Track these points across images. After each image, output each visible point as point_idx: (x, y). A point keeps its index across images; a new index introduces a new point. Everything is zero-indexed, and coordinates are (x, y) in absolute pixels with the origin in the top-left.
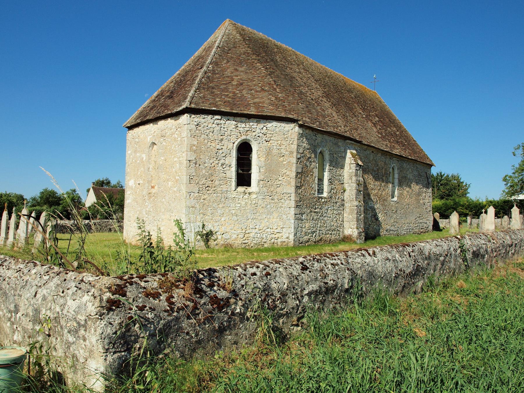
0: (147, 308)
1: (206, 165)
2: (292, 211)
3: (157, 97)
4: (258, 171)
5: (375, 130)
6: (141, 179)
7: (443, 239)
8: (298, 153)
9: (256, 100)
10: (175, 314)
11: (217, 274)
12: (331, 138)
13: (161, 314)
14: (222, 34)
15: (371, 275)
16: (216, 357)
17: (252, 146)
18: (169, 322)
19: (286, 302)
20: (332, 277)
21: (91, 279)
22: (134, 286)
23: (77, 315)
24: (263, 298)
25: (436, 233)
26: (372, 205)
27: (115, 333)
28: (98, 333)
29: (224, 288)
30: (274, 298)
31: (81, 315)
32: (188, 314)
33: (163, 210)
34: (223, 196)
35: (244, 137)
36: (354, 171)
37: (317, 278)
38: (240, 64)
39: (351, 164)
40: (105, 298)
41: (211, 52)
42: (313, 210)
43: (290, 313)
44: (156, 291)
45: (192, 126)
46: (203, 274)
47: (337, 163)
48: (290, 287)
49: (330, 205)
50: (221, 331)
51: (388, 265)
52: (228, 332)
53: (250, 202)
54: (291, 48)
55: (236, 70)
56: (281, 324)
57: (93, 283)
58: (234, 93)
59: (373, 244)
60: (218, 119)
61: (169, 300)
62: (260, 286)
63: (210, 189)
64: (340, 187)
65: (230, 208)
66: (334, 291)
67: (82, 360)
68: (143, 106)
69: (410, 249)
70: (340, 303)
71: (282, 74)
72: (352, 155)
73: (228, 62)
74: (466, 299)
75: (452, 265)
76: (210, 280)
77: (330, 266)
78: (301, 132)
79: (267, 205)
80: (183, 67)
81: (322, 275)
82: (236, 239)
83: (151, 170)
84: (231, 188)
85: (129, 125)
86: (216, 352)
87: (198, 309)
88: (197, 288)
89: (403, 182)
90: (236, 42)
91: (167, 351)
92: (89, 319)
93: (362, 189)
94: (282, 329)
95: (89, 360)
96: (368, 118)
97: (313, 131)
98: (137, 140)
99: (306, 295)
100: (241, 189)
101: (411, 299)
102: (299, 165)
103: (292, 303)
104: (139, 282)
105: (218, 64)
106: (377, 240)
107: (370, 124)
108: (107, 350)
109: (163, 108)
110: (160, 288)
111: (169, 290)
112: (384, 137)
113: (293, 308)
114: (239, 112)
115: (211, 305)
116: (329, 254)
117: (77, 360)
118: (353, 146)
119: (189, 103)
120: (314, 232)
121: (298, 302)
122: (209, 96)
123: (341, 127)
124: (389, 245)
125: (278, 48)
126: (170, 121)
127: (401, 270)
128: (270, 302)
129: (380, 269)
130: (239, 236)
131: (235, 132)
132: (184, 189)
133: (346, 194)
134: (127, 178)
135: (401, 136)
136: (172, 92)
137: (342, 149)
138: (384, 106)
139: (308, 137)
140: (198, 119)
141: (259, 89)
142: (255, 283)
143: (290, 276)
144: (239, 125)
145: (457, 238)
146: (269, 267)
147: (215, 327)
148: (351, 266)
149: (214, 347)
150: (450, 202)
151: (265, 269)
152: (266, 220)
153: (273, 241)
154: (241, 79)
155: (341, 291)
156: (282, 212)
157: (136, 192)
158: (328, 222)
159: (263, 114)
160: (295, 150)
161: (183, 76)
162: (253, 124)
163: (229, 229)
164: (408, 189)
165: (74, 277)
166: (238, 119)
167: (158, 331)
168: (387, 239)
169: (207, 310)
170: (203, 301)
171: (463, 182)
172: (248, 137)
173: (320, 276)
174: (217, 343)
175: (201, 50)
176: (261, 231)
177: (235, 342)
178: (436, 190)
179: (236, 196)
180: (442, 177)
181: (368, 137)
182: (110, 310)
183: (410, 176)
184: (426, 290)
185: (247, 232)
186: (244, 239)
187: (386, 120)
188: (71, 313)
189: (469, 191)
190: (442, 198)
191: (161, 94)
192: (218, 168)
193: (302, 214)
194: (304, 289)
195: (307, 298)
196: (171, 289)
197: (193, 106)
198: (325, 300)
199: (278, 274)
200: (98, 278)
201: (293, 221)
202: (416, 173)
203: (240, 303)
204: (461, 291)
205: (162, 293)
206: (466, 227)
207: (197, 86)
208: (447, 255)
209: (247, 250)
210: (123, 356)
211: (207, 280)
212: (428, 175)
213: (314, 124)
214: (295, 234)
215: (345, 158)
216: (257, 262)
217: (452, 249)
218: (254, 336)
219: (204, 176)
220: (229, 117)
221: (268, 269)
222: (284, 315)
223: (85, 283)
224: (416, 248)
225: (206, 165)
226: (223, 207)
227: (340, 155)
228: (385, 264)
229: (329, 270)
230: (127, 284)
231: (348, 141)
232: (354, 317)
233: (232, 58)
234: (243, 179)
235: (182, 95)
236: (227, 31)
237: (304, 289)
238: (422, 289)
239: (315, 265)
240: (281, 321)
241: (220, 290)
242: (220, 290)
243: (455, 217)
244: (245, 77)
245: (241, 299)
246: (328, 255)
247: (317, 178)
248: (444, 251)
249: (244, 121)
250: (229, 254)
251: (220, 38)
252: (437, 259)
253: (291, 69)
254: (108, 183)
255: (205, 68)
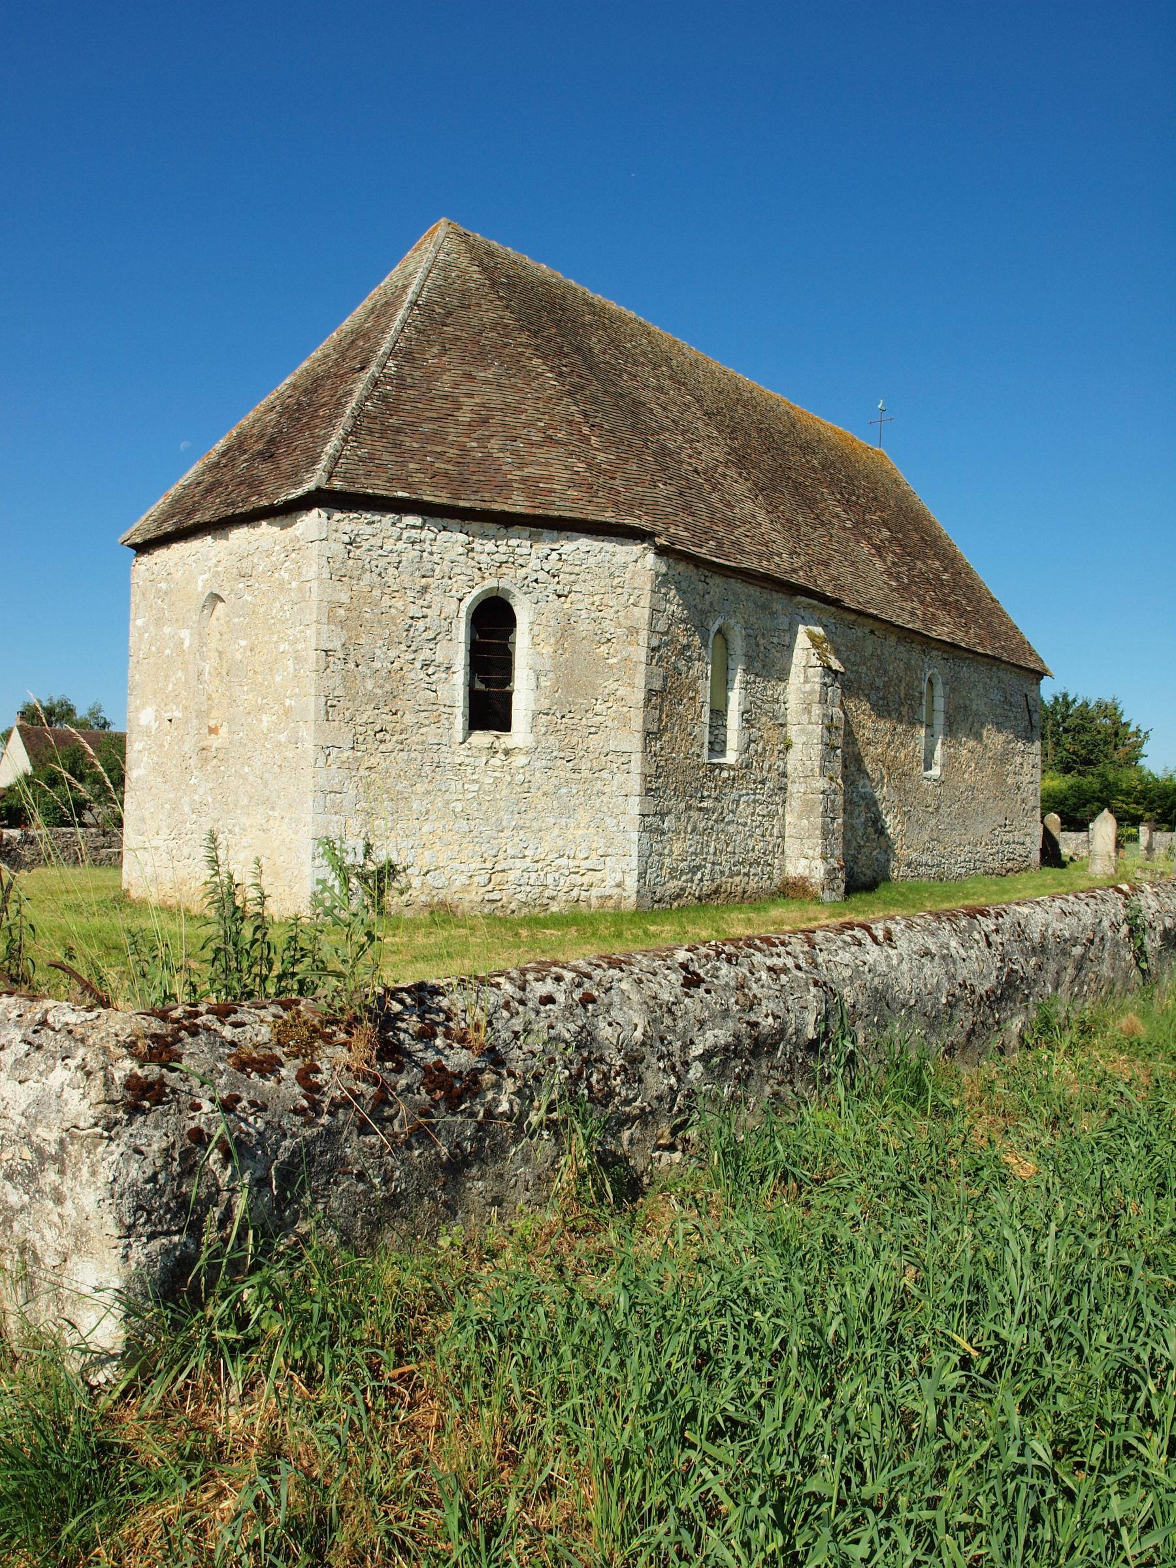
0: (244, 1103)
1: (377, 665)
2: (634, 806)
3: (224, 454)
4: (533, 686)
5: (879, 565)
6: (177, 705)
7: (1082, 895)
8: (652, 631)
9: (529, 471)
10: (325, 1119)
11: (445, 1003)
12: (752, 590)
13: (285, 1121)
14: (425, 265)
15: (881, 1000)
16: (444, 1242)
17: (516, 609)
18: (309, 1143)
19: (640, 1081)
20: (771, 1005)
21: (72, 1018)
22: (203, 1037)
23: (35, 1127)
24: (574, 1068)
25: (1051, 873)
26: (868, 789)
27: (153, 1179)
28: (101, 1180)
29: (463, 1041)
30: (605, 1068)
31: (48, 1126)
32: (363, 1120)
33: (246, 801)
34: (427, 760)
35: (491, 583)
36: (817, 687)
37: (727, 1010)
38: (482, 358)
39: (807, 666)
40: (119, 1075)
41: (391, 318)
42: (695, 803)
43: (651, 1113)
44: (268, 1052)
45: (333, 545)
46: (401, 1002)
47: (769, 664)
48: (651, 1038)
49: (744, 788)
50: (456, 1168)
51: (927, 971)
52: (474, 1170)
53: (508, 778)
54: (632, 314)
55: (469, 377)
56: (625, 1143)
57: (80, 1030)
58: (462, 448)
59: (871, 904)
60: (414, 527)
61: (304, 1077)
62: (567, 1036)
63: (388, 737)
64: (775, 734)
65: (447, 796)
66: (775, 1047)
67: (50, 1260)
68: (181, 482)
69: (989, 924)
70: (791, 1082)
71: (606, 392)
72: (812, 640)
73: (444, 351)
74: (1146, 1067)
75: (1105, 970)
76: (422, 1017)
77: (764, 975)
78: (664, 570)
79: (557, 788)
80: (305, 364)
81: (742, 1000)
82: (465, 888)
83: (207, 676)
84: (451, 736)
85: (139, 540)
86: (443, 1229)
87: (390, 1105)
88: (385, 1042)
89: (960, 722)
90: (469, 290)
91: (303, 1227)
92: (73, 1137)
93: (839, 742)
94: (627, 1159)
95: (75, 1258)
96: (860, 530)
97: (697, 566)
98: (163, 585)
99: (695, 1058)
100: (481, 738)
101: (990, 1068)
102: (656, 670)
103: (657, 1082)
104: (216, 1025)
105: (414, 359)
106: (882, 892)
107: (865, 549)
108: (130, 1228)
109: (245, 491)
110: (280, 1043)
111: (304, 1049)
112: (906, 588)
113: (660, 1099)
114: (479, 505)
115: (428, 1093)
116: (762, 940)
117: (37, 1259)
118: (816, 615)
119: (325, 476)
120: (699, 868)
121: (673, 1080)
122: (386, 456)
123: (780, 555)
124: (930, 913)
125: (594, 314)
126: (266, 531)
127: (963, 986)
128: (594, 1079)
129: (906, 983)
130: (475, 879)
131: (465, 567)
132: (308, 738)
133: (793, 757)
134: (134, 701)
135: (955, 586)
136: (272, 441)
137: (783, 622)
138: (906, 495)
139: (684, 585)
140: (353, 526)
141: (538, 437)
142: (551, 1027)
143: (652, 1003)
144: (477, 544)
145: (1120, 891)
146: (589, 977)
147: (438, 1154)
148: (824, 976)
149: (436, 1213)
150: (1090, 782)
151: (579, 985)
152: (556, 831)
153: (575, 893)
154: (483, 405)
155: (796, 1046)
156: (605, 809)
157: (162, 746)
158: (739, 838)
159: (550, 513)
160: (643, 625)
161: (306, 392)
162: (519, 544)
163: (441, 858)
164: (971, 743)
165: (16, 1012)
166: (475, 526)
167: (277, 1170)
168: (910, 889)
169: (417, 1105)
170: (403, 1082)
171: (1127, 725)
172: (504, 583)
173: (737, 1002)
174: (445, 1203)
175: (360, 311)
176: (539, 865)
177: (494, 1198)
178: (1050, 745)
179: (467, 761)
180: (1067, 708)
181: (860, 586)
182: (134, 1110)
183: (979, 705)
184: (1031, 1042)
185: (498, 867)
186: (489, 888)
187: (912, 538)
188: (13, 1122)
189: (1144, 751)
190: (1067, 769)
191: (239, 446)
192: (412, 675)
193: (662, 815)
194: (692, 1043)
195: (701, 1068)
196: (310, 1045)
197: (337, 484)
198: (749, 1074)
199: (616, 999)
200: (94, 1014)
201: (635, 836)
202: (997, 697)
203: (509, 1085)
204: (1131, 1044)
205: (283, 1058)
206: (1135, 854)
207: (351, 422)
208: (1091, 942)
209: (503, 922)
210: (175, 1246)
211: (415, 1018)
212: (1031, 703)
213: (701, 547)
214: (642, 876)
215: (790, 648)
216: (555, 963)
217: (1106, 923)
218: (550, 1181)
219: (370, 697)
220: (446, 522)
221: (587, 984)
222: (635, 1118)
223: (53, 1029)
224: (1006, 921)
225: (377, 665)
226: (428, 792)
227: (775, 640)
228: (921, 969)
229: (762, 986)
230: (183, 1033)
231: (800, 598)
232: (830, 1121)
233: (457, 338)
234: (489, 709)
235: (304, 451)
236: (441, 256)
237: (692, 1043)
238: (1021, 1038)
239: (723, 972)
240: (626, 1135)
241: (452, 1048)
242: (452, 1048)
243: (1104, 827)
244: (494, 398)
245: (511, 1074)
246: (758, 942)
247: (707, 709)
248: (1085, 928)
249: (491, 533)
250: (446, 934)
251: (419, 276)
252: (1065, 953)
253: (634, 377)
254: (70, 711)
255: (373, 369)
